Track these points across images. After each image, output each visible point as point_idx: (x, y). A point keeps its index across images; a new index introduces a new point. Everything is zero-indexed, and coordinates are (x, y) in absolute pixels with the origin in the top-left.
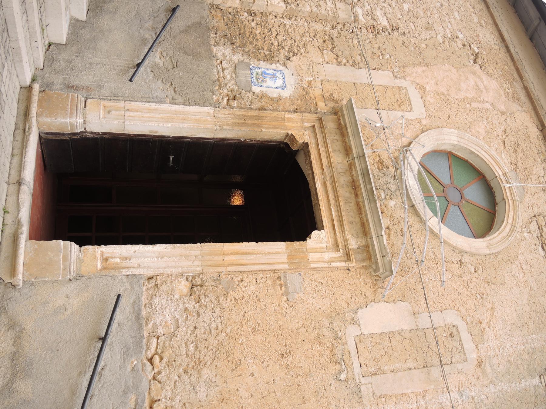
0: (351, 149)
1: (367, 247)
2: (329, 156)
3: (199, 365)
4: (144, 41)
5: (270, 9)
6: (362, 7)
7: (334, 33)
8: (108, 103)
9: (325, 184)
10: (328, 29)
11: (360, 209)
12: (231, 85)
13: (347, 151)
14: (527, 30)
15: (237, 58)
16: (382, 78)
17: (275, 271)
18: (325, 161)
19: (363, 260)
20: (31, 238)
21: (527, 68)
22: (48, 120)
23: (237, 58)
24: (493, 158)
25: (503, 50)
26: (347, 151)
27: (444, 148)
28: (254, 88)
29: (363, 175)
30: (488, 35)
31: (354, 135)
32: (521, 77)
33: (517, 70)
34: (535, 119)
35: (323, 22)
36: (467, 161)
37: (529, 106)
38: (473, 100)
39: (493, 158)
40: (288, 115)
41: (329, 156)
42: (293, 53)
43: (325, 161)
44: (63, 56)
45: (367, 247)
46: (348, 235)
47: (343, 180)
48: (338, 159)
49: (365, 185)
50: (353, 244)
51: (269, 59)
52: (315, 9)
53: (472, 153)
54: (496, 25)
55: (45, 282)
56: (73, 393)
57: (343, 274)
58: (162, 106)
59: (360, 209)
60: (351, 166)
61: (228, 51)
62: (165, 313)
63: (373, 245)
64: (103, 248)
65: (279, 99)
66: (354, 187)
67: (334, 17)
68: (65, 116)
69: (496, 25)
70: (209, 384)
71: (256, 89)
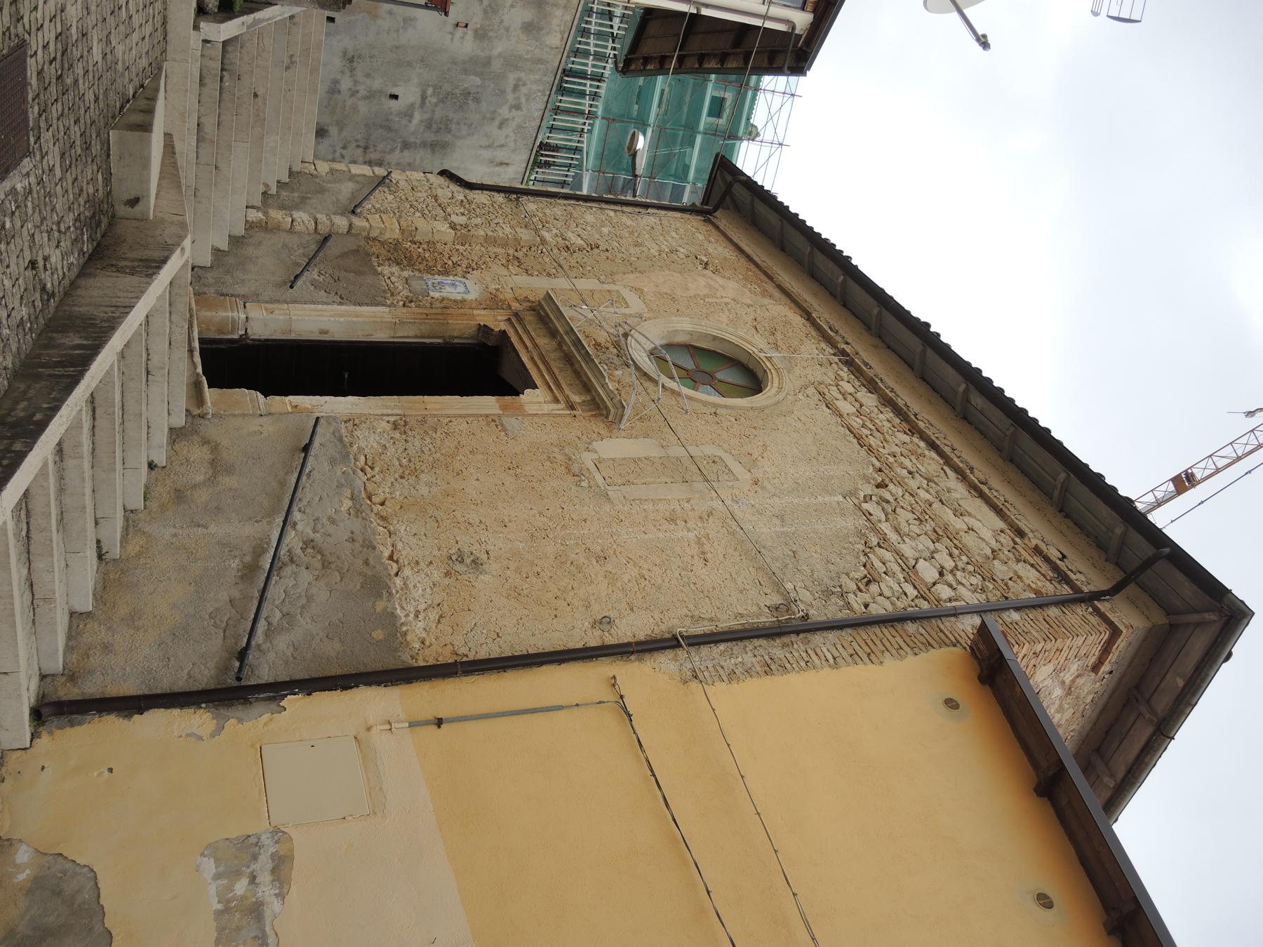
0: (557, 331)
1: (593, 400)
2: (532, 339)
3: (415, 473)
4: (298, 264)
5: (437, 237)
6: (549, 230)
7: (520, 254)
8: (270, 306)
9: (532, 359)
10: (511, 251)
11: (578, 374)
12: (406, 293)
13: (553, 333)
14: (833, 295)
15: (406, 274)
16: (585, 284)
17: (487, 416)
18: (529, 344)
19: (590, 410)
20: (210, 387)
21: (898, 389)
22: (209, 314)
23: (406, 274)
24: (742, 338)
25: (743, 260)
26: (553, 333)
27: (680, 339)
28: (432, 294)
29: (575, 345)
30: (720, 249)
31: (558, 319)
32: (771, 278)
33: (766, 273)
34: (797, 310)
35: (505, 245)
36: (714, 352)
37: (784, 299)
38: (707, 296)
39: (742, 338)
40: (476, 312)
41: (532, 339)
42: (470, 268)
43: (529, 344)
44: (210, 277)
45: (593, 400)
46: (567, 392)
47: (552, 357)
48: (544, 342)
49: (579, 352)
50: (576, 399)
51: (446, 272)
52: (490, 233)
53: (715, 338)
54: (731, 241)
55: (234, 415)
56: (282, 484)
57: (568, 420)
58: (330, 307)
59: (578, 374)
60: (560, 345)
61: (395, 269)
62: (367, 441)
63: (599, 395)
64: (291, 398)
65: (463, 301)
66: (568, 359)
67: (516, 239)
68: (226, 310)
69: (731, 241)
70: (428, 484)
71: (436, 295)
